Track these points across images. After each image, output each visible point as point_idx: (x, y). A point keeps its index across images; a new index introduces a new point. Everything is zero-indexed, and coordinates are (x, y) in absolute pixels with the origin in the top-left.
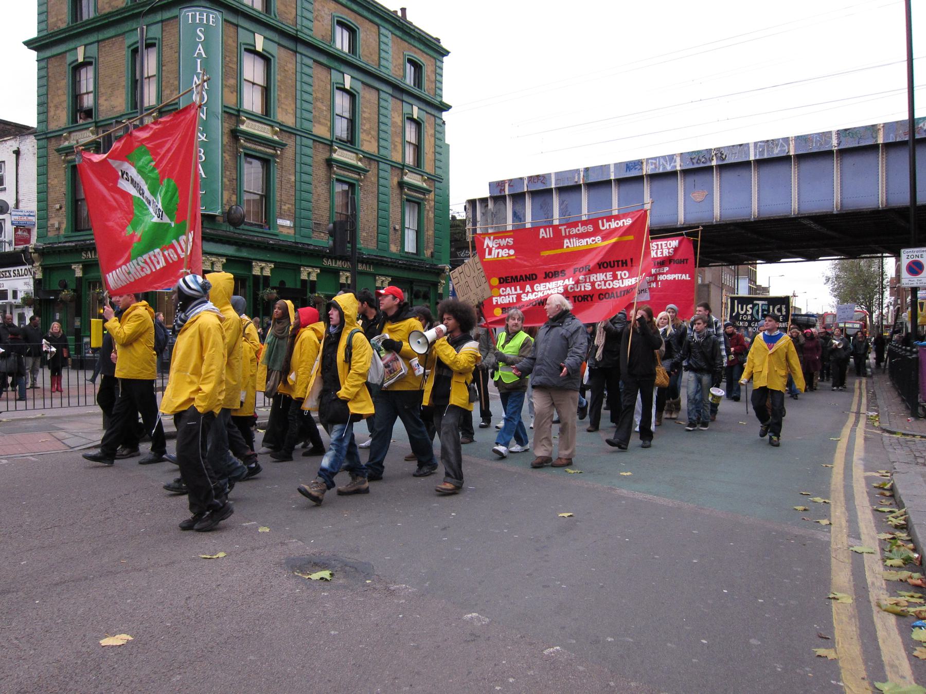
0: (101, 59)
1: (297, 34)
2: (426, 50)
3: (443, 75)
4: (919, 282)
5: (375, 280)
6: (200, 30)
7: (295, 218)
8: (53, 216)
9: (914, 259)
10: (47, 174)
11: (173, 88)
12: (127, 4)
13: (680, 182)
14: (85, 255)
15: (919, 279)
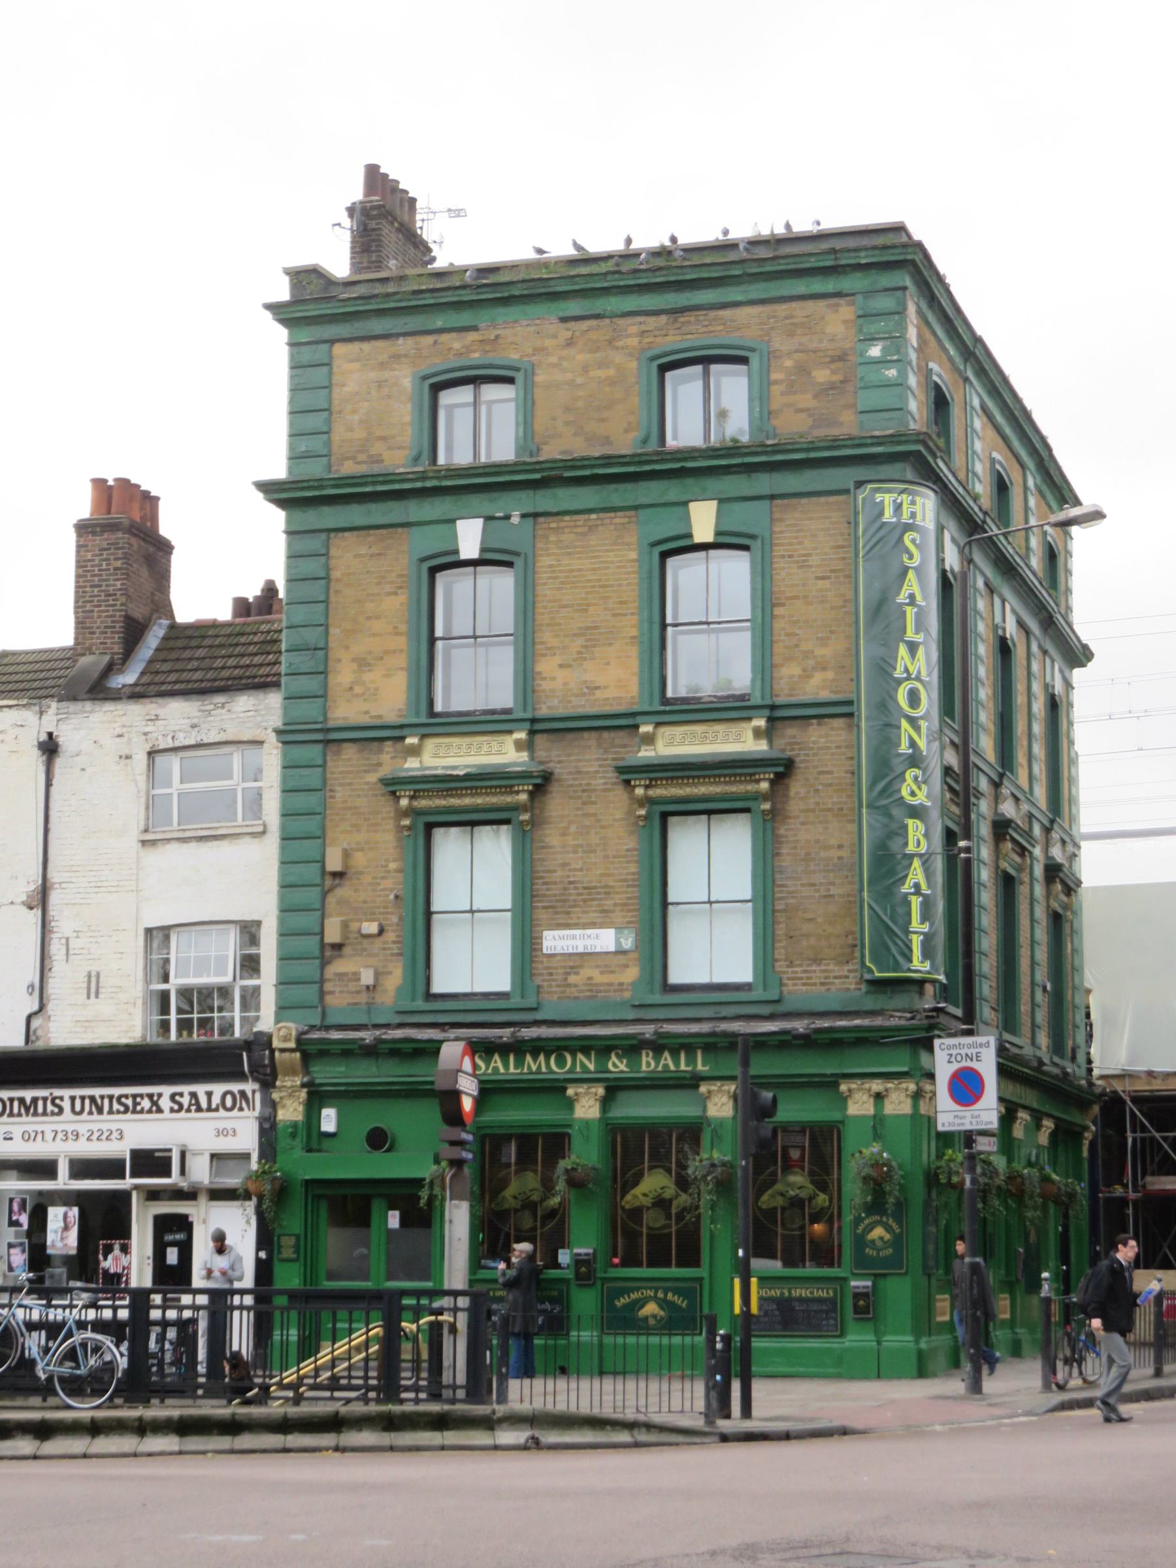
0: (544, 561)
1: (984, 522)
4: (974, 1121)
6: (913, 541)
9: (964, 1064)
11: (811, 662)
15: (976, 1113)
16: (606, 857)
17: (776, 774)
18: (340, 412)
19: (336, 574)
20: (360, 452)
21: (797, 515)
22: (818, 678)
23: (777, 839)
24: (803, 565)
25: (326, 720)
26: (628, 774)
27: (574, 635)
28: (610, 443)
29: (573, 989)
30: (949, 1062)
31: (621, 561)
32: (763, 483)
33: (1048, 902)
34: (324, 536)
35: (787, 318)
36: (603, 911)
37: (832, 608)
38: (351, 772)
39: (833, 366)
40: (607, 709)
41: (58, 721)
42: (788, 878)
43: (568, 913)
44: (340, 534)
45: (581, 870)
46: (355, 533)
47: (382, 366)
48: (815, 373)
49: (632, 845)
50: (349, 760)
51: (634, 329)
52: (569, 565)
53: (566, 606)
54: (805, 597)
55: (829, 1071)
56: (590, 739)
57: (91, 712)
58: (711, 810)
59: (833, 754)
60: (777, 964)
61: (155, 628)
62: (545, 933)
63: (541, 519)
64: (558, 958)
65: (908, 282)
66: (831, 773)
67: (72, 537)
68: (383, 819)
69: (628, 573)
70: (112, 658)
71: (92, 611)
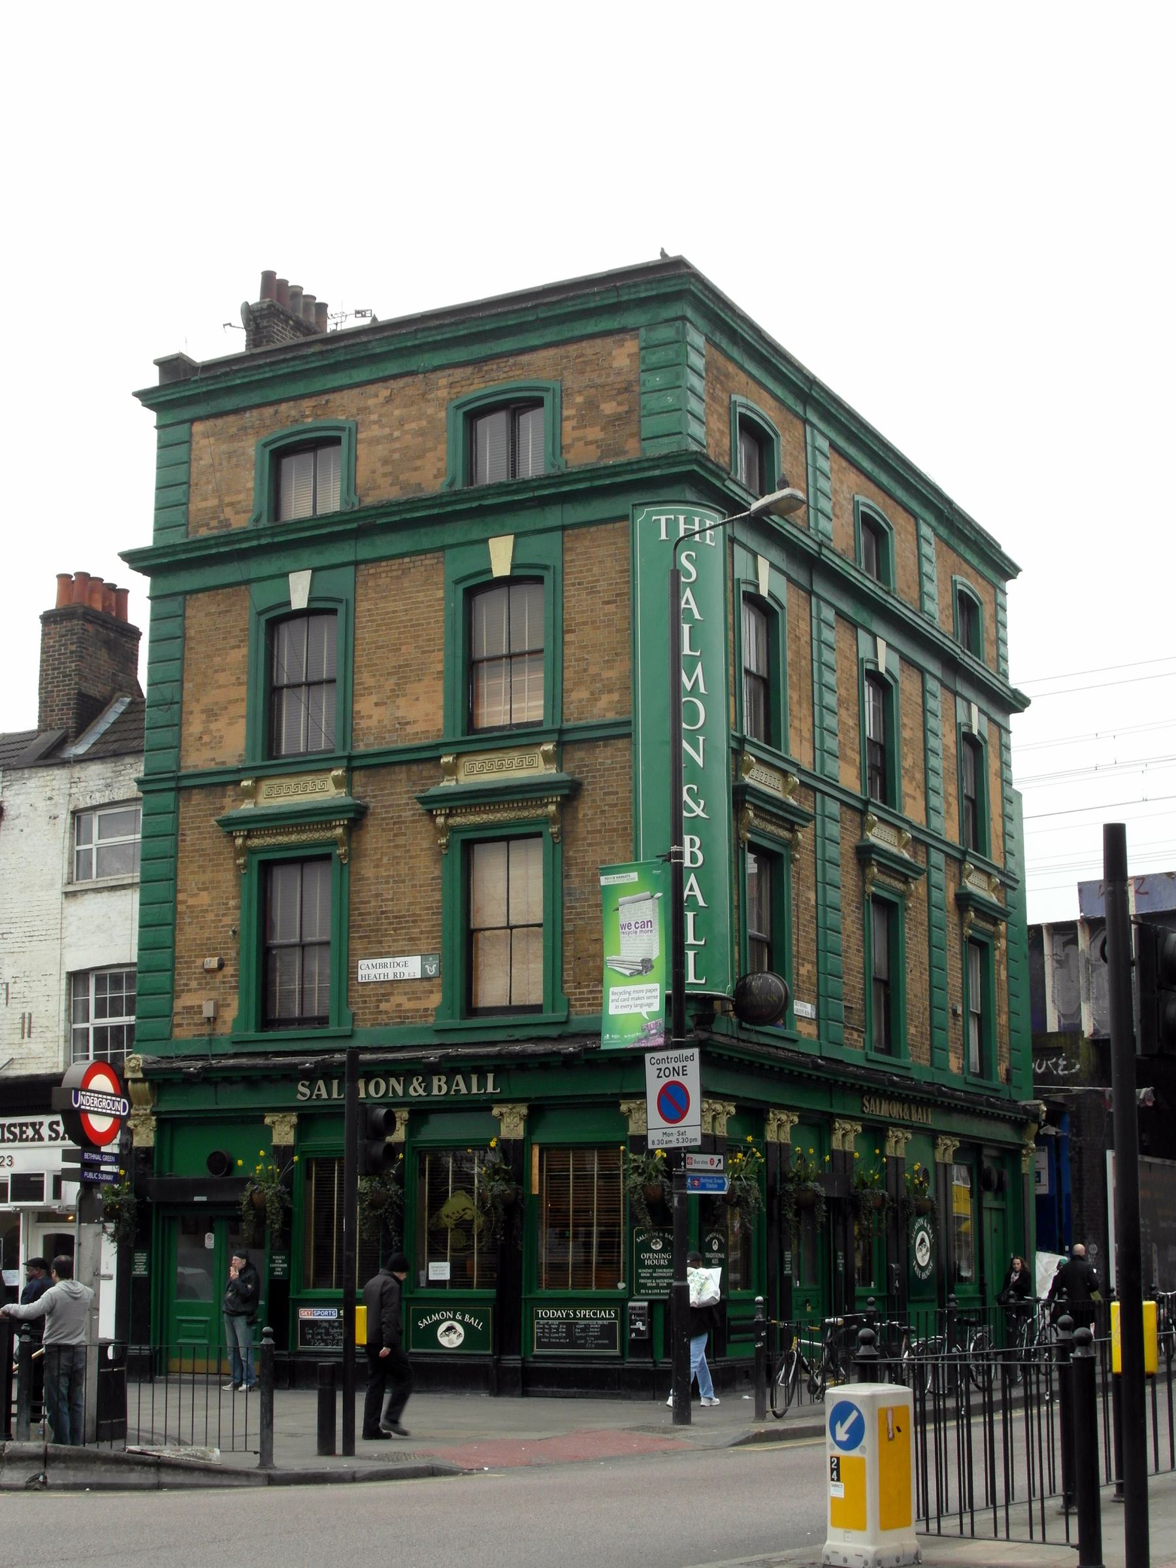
0: (363, 606)
1: (820, 553)
2: (981, 568)
3: (1009, 626)
5: (935, 1146)
6: (688, 557)
7: (818, 995)
8: (194, 984)
9: (671, 1079)
10: (174, 879)
12: (451, 484)
13: (324, 685)
14: (308, 1092)
15: (682, 1130)
16: (414, 886)
17: (562, 796)
18: (197, 484)
19: (191, 633)
20: (213, 518)
21: (587, 543)
22: (605, 700)
23: (566, 862)
24: (592, 591)
25: (179, 768)
26: (431, 804)
27: (389, 674)
28: (422, 490)
29: (384, 1016)
30: (658, 1077)
31: (430, 601)
32: (554, 516)
33: (962, 929)
34: (180, 598)
35: (578, 357)
36: (411, 939)
37: (618, 631)
38: (199, 817)
39: (619, 398)
40: (416, 743)
41: (3, 788)
42: (577, 900)
43: (380, 942)
44: (194, 596)
45: (392, 899)
46: (207, 593)
47: (232, 438)
48: (603, 406)
49: (437, 873)
50: (199, 804)
51: (443, 382)
52: (384, 608)
53: (382, 647)
54: (592, 622)
55: (609, 1092)
56: (401, 774)
57: (28, 779)
58: (507, 837)
59: (617, 775)
60: (566, 986)
61: (117, 705)
62: (360, 962)
63: (362, 567)
64: (372, 986)
65: (689, 313)
66: (617, 793)
67: (38, 626)
68: (224, 859)
69: (436, 611)
70: (67, 731)
71: (53, 691)
